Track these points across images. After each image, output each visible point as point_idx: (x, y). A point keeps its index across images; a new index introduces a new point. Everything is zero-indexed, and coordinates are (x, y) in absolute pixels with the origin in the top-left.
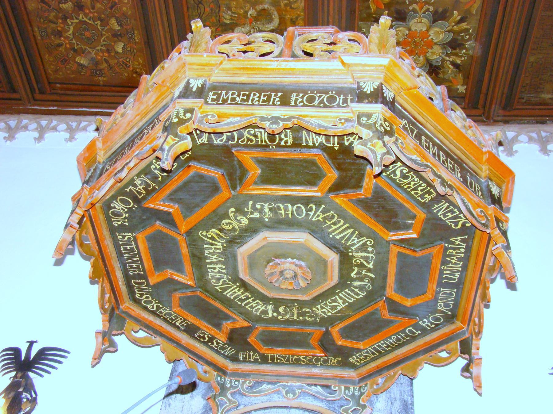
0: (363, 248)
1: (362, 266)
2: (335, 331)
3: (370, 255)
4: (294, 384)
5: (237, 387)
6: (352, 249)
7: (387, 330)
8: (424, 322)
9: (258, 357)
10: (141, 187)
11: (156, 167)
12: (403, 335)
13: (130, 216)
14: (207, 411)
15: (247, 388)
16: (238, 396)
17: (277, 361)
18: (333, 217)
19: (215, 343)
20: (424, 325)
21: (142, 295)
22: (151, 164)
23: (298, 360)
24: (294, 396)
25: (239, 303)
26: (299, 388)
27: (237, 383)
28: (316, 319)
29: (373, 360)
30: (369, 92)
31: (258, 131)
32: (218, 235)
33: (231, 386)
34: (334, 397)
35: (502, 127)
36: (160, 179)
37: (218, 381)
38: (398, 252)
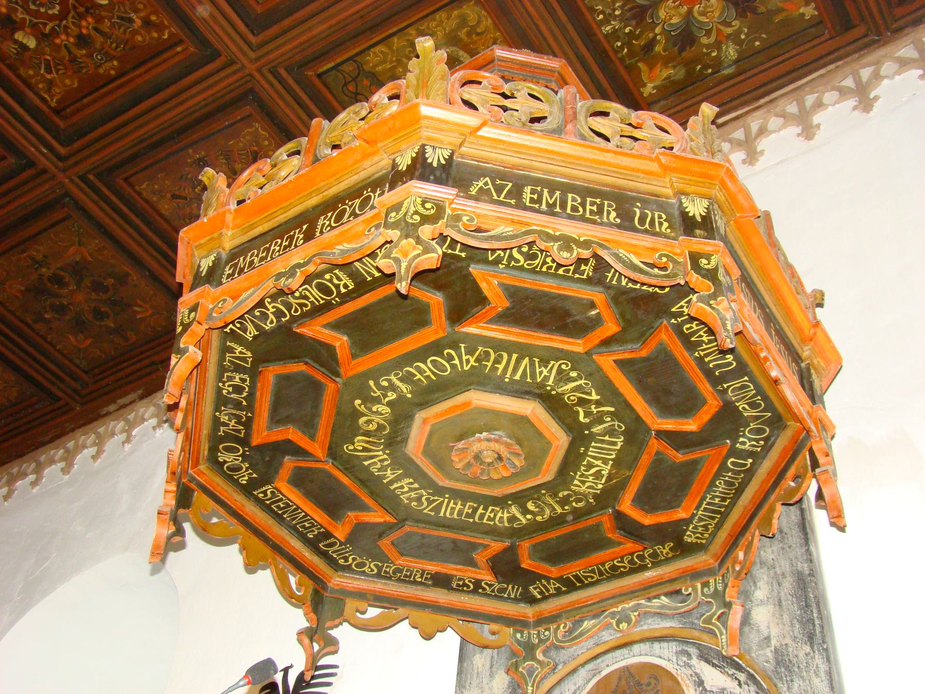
0: (562, 377)
1: (582, 402)
2: (626, 505)
3: (582, 382)
4: (627, 606)
5: (548, 639)
6: (549, 385)
7: (699, 476)
8: (743, 443)
9: (558, 585)
10: (233, 423)
11: (228, 390)
12: (730, 474)
13: (250, 464)
14: (514, 690)
15: (564, 636)
16: (553, 653)
17: (587, 580)
18: (487, 354)
19: (487, 588)
20: (747, 447)
21: (346, 559)
22: (219, 390)
23: (614, 568)
24: (629, 625)
25: (471, 520)
26: (634, 609)
27: (547, 633)
28: (588, 501)
29: (718, 527)
30: (404, 169)
31: (303, 290)
32: (368, 442)
33: (540, 641)
34: (688, 605)
35: (913, 34)
36: (244, 403)
37: (518, 641)
38: (615, 361)
